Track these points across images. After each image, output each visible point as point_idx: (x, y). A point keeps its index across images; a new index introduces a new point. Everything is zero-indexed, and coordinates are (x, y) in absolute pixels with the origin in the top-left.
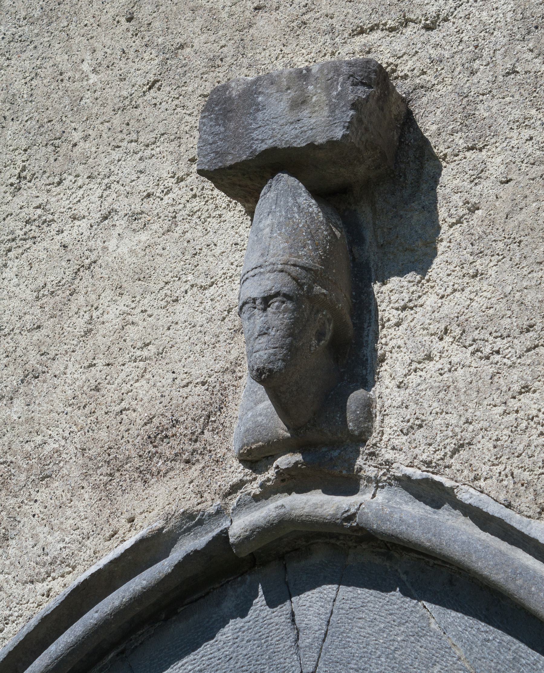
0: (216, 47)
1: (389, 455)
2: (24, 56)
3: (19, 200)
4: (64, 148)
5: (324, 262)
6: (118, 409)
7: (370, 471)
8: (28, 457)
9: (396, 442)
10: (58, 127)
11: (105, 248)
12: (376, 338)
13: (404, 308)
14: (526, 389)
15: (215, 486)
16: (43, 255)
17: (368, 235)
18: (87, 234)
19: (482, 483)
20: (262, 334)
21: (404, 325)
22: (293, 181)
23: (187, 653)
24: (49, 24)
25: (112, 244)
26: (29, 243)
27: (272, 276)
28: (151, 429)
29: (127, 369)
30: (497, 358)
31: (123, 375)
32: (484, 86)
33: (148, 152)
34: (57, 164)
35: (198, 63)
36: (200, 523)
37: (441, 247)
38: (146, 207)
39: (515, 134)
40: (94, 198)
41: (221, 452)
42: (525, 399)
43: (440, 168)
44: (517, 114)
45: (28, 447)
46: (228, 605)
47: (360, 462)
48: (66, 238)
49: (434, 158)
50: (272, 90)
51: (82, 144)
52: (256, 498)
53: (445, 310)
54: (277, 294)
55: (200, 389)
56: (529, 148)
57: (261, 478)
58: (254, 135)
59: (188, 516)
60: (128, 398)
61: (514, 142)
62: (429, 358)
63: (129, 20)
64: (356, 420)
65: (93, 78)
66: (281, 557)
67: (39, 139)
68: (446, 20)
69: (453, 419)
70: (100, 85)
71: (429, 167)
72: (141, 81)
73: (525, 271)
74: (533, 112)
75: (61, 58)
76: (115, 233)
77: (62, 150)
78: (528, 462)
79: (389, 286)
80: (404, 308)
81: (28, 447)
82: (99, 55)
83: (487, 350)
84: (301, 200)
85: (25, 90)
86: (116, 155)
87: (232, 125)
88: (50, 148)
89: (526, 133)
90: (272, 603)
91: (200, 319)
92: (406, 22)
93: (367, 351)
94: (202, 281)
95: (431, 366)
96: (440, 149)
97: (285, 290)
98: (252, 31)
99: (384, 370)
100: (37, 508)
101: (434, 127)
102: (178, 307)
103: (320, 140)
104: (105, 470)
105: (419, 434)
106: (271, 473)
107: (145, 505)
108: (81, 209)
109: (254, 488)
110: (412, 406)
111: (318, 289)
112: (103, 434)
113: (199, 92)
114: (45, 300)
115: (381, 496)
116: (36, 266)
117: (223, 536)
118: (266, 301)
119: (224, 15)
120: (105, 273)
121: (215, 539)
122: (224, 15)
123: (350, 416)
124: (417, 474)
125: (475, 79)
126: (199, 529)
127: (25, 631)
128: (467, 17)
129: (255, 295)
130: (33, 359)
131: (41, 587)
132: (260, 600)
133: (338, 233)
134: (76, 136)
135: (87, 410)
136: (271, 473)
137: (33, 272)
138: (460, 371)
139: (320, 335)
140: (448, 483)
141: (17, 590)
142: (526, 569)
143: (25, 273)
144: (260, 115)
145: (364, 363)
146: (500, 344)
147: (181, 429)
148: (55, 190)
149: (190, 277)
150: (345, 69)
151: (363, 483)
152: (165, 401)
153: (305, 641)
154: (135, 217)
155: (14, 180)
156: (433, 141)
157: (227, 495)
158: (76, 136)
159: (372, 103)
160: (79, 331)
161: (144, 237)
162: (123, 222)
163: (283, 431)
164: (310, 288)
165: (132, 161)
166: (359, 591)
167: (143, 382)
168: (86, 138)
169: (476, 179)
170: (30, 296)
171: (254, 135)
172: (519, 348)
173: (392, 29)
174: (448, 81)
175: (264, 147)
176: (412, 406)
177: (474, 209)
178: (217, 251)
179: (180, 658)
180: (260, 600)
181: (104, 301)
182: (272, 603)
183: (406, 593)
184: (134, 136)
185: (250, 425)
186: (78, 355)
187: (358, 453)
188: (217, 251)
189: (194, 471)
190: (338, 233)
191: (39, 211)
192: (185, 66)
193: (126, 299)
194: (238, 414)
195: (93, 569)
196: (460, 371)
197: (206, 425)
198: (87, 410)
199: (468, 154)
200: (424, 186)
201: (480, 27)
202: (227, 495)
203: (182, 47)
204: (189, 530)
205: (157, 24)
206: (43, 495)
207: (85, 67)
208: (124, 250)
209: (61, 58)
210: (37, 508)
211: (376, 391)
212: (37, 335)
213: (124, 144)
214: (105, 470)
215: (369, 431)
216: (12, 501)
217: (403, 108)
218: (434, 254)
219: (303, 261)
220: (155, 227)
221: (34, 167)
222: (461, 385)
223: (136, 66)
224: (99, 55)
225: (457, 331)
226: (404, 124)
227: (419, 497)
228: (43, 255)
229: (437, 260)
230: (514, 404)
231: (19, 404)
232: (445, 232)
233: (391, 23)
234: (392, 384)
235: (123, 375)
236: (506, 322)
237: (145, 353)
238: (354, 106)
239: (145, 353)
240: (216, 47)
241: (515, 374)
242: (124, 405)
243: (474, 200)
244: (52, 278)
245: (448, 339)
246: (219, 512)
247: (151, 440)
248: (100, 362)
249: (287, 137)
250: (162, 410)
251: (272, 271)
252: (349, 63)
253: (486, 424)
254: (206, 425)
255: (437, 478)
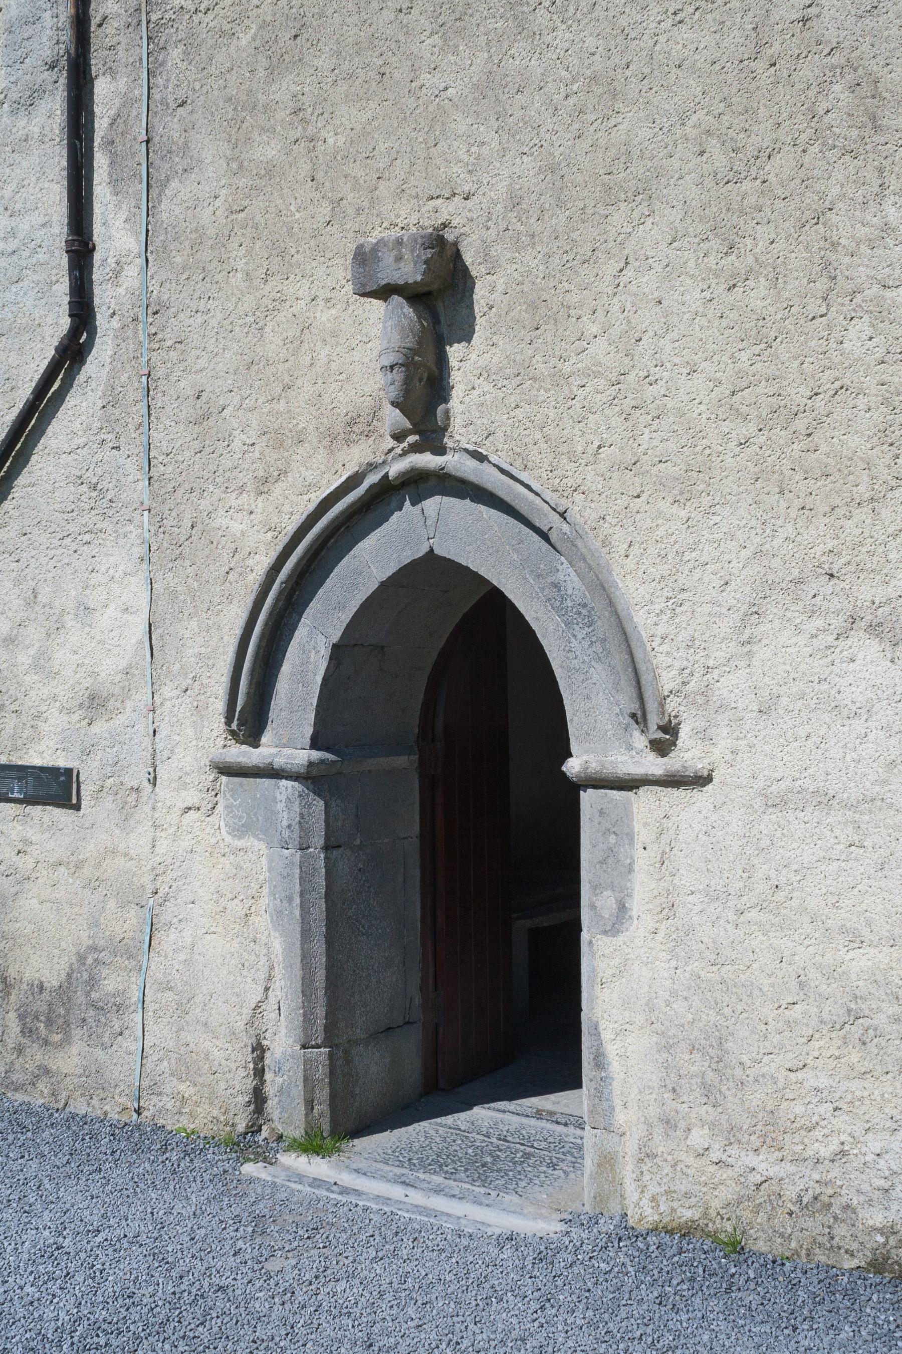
0: (359, 201)
1: (457, 437)
2: (259, 199)
3: (268, 288)
4: (288, 257)
5: (419, 343)
6: (331, 407)
7: (450, 444)
8: (291, 431)
9: (461, 431)
10: (282, 245)
11: (315, 317)
12: (449, 376)
13: (461, 361)
14: (517, 406)
15: (381, 449)
16: (284, 320)
17: (442, 319)
18: (305, 308)
19: (499, 453)
20: (391, 384)
21: (462, 370)
22: (400, 299)
23: (377, 528)
24: (270, 180)
25: (318, 315)
26: (276, 312)
27: (393, 354)
28: (348, 418)
29: (333, 386)
30: (504, 389)
31: (331, 389)
32: (493, 237)
33: (330, 263)
34: (285, 268)
35: (351, 211)
36: (376, 467)
37: (477, 328)
38: (333, 295)
39: (509, 266)
40: (306, 288)
41: (382, 431)
42: (517, 411)
43: (474, 283)
44: (509, 255)
45: (290, 426)
46: (393, 504)
47: (445, 440)
48: (294, 310)
49: (471, 277)
50: (385, 250)
51: (296, 255)
52: (400, 455)
53: (480, 363)
54: (397, 364)
55: (369, 398)
56: (516, 275)
57: (402, 446)
58: (379, 275)
59: (370, 464)
60: (335, 401)
61: (509, 272)
62: (474, 388)
63: (312, 181)
64: (442, 421)
65: (298, 215)
66: (415, 482)
67: (274, 252)
68: (473, 195)
69: (485, 421)
70: (301, 220)
71: (469, 283)
72: (322, 220)
73: (516, 344)
74: (517, 254)
75: (279, 202)
76: (319, 309)
77: (286, 259)
78: (519, 444)
79: (453, 348)
80: (461, 361)
81: (290, 426)
82: (299, 201)
83: (500, 386)
84: (405, 310)
85: (262, 221)
86: (314, 264)
87: (367, 269)
88: (280, 258)
89: (515, 266)
90: (413, 504)
91: (366, 360)
92: (454, 194)
93: (445, 383)
94: (365, 339)
95: (475, 392)
96: (474, 273)
97: (400, 361)
98: (377, 192)
99: (454, 393)
100: (299, 457)
101: (470, 260)
102: (355, 353)
103: (411, 281)
104: (328, 439)
105: (471, 428)
106: (405, 444)
107: (349, 458)
108: (300, 294)
109: (399, 451)
110: (467, 414)
111: (417, 358)
112: (325, 420)
113: (353, 229)
114: (288, 345)
115: (457, 456)
116: (281, 326)
117: (386, 476)
118: (392, 367)
119: (362, 182)
120: (317, 331)
121: (383, 477)
122: (362, 182)
123: (439, 419)
124: (471, 448)
125: (489, 232)
126: (375, 470)
127: (301, 521)
128: (484, 194)
129: (386, 364)
130: (287, 379)
131: (306, 497)
132: (408, 503)
133: (425, 324)
134: (293, 251)
135: (316, 407)
136: (405, 444)
137: (280, 329)
138: (488, 396)
139: (421, 380)
140: (485, 453)
141: (294, 498)
142: (520, 494)
143: (276, 330)
144: (380, 264)
145: (444, 389)
146: (505, 382)
147: (361, 419)
148: (286, 282)
149: (359, 337)
150: (420, 240)
151: (448, 450)
152: (353, 404)
153: (429, 523)
154: (328, 300)
155: (263, 276)
156: (470, 268)
157: (386, 454)
158: (293, 251)
159: (435, 257)
160: (307, 364)
161: (333, 311)
162: (322, 303)
163: (409, 426)
164: (413, 358)
165: (323, 268)
166: (452, 499)
167: (341, 393)
168: (298, 252)
169: (492, 291)
170: (281, 344)
171: (379, 275)
172: (514, 385)
173: (447, 199)
174: (476, 232)
175: (384, 283)
176: (467, 414)
177: (491, 308)
178: (371, 322)
179: (374, 530)
180: (408, 503)
181: (318, 348)
182: (413, 504)
183: (472, 500)
184: (322, 254)
185: (393, 421)
186: (308, 377)
187: (444, 436)
188: (371, 322)
189: (370, 441)
190: (425, 324)
191: (279, 295)
192: (344, 212)
193: (328, 347)
194: (388, 413)
195: (328, 492)
196: (488, 396)
197: (373, 417)
198: (316, 407)
199: (487, 277)
200: (467, 294)
201: (491, 201)
202: (386, 454)
203: (342, 199)
204: (371, 470)
205: (327, 184)
206: (301, 450)
207: (292, 208)
208: (324, 319)
209: (279, 202)
210: (299, 457)
211: (451, 404)
212: (287, 365)
213: (318, 258)
214: (328, 439)
215: (449, 425)
216: (286, 454)
217: (454, 249)
218: (474, 333)
219: (408, 345)
220: (339, 307)
221: (273, 269)
222: (488, 403)
223: (319, 210)
224: (299, 201)
225: (486, 375)
226: (456, 257)
227: (473, 457)
228: (284, 320)
229: (475, 336)
230: (512, 414)
231: (282, 402)
232: (478, 320)
233: (447, 195)
234: (458, 401)
235: (331, 389)
236: (507, 371)
237: (341, 378)
238: (425, 262)
239: (341, 378)
240: (359, 201)
241: (513, 398)
242: (334, 405)
243: (491, 303)
244: (290, 334)
245: (482, 378)
246: (384, 462)
247: (349, 424)
248: (320, 381)
249: (395, 278)
250: (352, 409)
251: (393, 351)
252: (422, 237)
253: (500, 424)
254: (373, 417)
255: (480, 450)
